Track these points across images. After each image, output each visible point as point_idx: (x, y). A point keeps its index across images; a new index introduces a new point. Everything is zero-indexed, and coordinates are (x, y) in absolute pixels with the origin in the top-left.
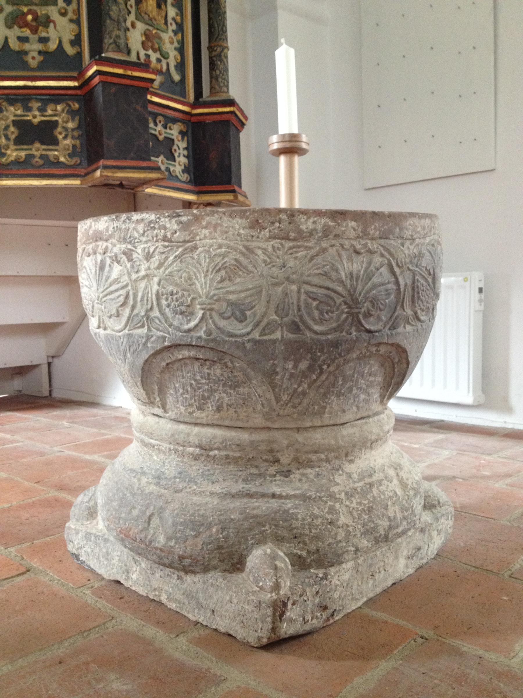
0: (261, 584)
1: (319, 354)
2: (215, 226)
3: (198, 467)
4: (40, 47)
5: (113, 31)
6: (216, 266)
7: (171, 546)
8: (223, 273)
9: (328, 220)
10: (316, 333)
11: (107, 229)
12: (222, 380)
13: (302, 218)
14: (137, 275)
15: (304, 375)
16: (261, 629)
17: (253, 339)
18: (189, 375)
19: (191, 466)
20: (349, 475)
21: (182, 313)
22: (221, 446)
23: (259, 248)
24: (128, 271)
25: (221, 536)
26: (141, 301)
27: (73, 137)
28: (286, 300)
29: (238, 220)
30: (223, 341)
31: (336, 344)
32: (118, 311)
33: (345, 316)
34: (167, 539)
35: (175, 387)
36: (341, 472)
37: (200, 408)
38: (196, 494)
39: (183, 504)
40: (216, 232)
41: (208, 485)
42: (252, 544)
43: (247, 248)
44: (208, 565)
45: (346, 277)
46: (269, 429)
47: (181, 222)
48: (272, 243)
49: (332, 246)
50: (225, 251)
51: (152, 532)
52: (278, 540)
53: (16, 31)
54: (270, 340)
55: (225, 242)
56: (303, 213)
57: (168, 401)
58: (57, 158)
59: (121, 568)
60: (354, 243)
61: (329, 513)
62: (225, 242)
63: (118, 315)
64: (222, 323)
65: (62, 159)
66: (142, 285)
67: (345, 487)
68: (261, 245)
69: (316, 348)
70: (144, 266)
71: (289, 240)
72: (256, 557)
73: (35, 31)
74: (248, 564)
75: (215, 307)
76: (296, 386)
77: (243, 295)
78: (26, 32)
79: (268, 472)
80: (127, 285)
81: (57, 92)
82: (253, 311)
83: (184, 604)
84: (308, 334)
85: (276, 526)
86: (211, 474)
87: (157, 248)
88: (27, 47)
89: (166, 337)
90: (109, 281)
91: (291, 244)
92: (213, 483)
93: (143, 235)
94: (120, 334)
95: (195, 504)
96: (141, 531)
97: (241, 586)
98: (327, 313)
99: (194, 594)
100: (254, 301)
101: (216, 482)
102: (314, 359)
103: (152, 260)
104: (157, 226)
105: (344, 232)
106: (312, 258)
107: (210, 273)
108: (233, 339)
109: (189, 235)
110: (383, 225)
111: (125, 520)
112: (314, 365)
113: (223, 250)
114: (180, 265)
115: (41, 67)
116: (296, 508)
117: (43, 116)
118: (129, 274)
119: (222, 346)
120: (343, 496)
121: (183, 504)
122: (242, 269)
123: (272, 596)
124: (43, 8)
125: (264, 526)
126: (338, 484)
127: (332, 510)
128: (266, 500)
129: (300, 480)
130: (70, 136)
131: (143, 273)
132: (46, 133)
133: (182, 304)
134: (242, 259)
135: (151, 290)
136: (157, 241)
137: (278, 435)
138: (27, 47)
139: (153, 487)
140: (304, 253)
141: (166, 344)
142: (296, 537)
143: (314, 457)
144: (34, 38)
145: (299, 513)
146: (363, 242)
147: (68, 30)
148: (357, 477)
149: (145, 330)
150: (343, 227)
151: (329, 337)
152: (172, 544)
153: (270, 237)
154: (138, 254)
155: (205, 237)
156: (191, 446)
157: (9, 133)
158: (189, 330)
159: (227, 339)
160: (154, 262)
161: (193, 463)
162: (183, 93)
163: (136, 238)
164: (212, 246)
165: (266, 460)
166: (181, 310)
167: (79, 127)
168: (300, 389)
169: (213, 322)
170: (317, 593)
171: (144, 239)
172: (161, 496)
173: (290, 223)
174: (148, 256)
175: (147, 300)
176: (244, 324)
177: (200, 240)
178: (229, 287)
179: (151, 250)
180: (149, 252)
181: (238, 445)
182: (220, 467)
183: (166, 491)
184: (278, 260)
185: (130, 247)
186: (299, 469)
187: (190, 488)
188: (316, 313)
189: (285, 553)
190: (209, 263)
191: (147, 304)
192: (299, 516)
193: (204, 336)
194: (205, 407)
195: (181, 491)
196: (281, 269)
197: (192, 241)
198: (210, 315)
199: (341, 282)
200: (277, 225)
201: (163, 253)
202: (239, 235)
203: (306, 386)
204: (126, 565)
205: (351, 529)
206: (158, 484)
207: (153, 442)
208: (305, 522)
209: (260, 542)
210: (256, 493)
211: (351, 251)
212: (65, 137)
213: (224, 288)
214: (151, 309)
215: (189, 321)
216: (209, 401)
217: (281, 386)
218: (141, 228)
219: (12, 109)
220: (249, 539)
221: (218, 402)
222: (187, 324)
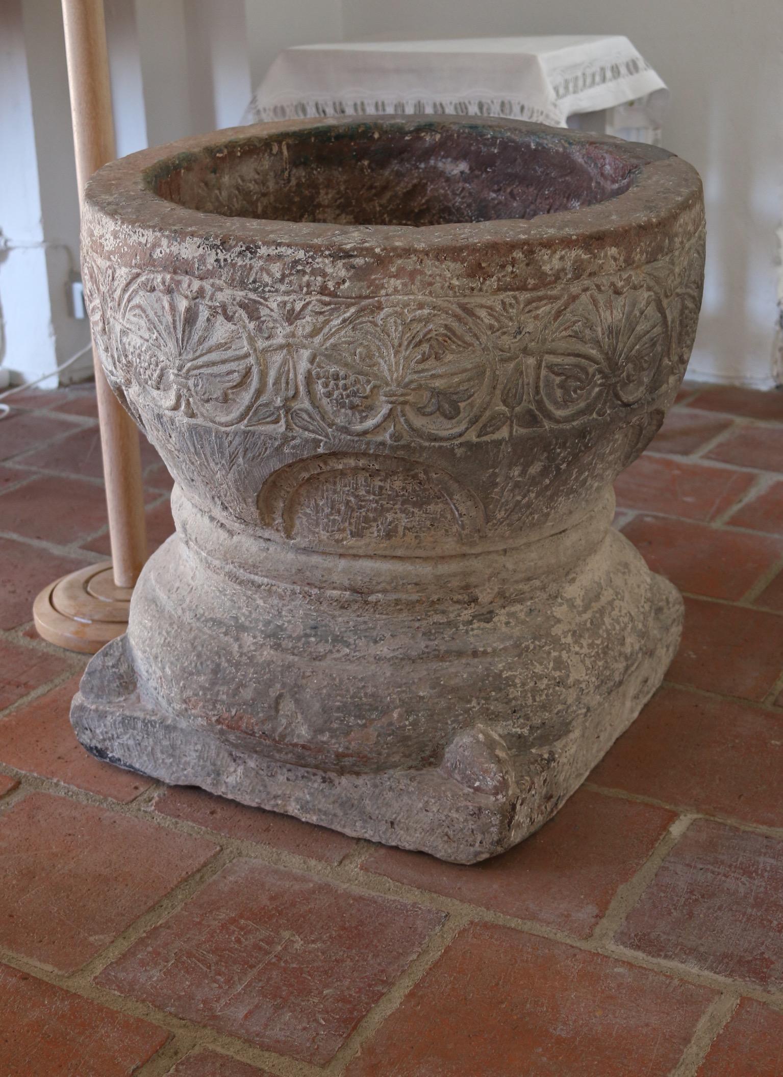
0: (477, 784)
1: (558, 450)
2: (412, 275)
3: (346, 619)
6: (413, 337)
7: (322, 742)
8: (425, 347)
9: (580, 252)
10: (558, 422)
11: (202, 259)
12: (403, 495)
13: (544, 254)
14: (267, 343)
15: (534, 481)
16: (481, 842)
17: (468, 442)
18: (347, 489)
19: (334, 617)
20: (571, 603)
21: (353, 407)
22: (388, 587)
23: (482, 306)
24: (249, 334)
25: (407, 723)
26: (274, 384)
28: (520, 381)
29: (450, 263)
30: (421, 447)
31: (582, 433)
32: (226, 394)
33: (597, 389)
34: (315, 731)
35: (317, 505)
36: (559, 600)
37: (357, 534)
38: (351, 662)
39: (334, 679)
40: (413, 283)
41: (367, 645)
42: (454, 728)
43: (463, 307)
44: (385, 763)
45: (603, 334)
46: (464, 555)
47: (353, 267)
48: (501, 297)
49: (585, 290)
50: (430, 314)
51: (284, 721)
52: (490, 719)
54: (492, 441)
55: (429, 299)
56: (545, 247)
57: (297, 522)
59: (203, 768)
60: (615, 279)
61: (554, 669)
62: (429, 299)
63: (226, 399)
64: (419, 422)
66: (278, 358)
67: (570, 623)
68: (483, 301)
69: (556, 444)
71: (526, 290)
72: (462, 745)
74: (447, 756)
75: (410, 398)
76: (519, 498)
77: (456, 379)
79: (461, 619)
80: (247, 356)
82: (469, 401)
83: (335, 815)
84: (547, 425)
85: (487, 699)
86: (369, 628)
87: (308, 304)
89: (321, 441)
90: (206, 345)
91: (528, 295)
92: (376, 642)
93: (281, 281)
94: (228, 429)
95: (354, 678)
96: (263, 722)
97: (443, 788)
98: (575, 392)
99: (356, 802)
100: (473, 386)
101: (381, 639)
102: (551, 459)
103: (299, 322)
104: (308, 271)
105: (601, 267)
106: (559, 313)
107: (403, 347)
108: (437, 444)
109: (368, 287)
110: (651, 242)
111: (229, 706)
112: (550, 466)
113: (426, 311)
114: (352, 334)
116: (510, 669)
118: (251, 340)
119: (418, 455)
120: (569, 639)
121: (334, 679)
122: (455, 339)
123: (497, 800)
125: (469, 702)
126: (559, 621)
127: (559, 664)
128: (464, 661)
129: (507, 623)
131: (279, 340)
133: (355, 394)
134: (455, 325)
135: (295, 368)
136: (309, 293)
137: (476, 564)
139: (267, 653)
140: (548, 308)
141: (320, 450)
142: (515, 712)
143: (525, 587)
145: (515, 676)
146: (625, 276)
148: (581, 604)
149: (281, 427)
150: (600, 259)
151: (575, 423)
152: (325, 739)
153: (499, 289)
154: (272, 310)
155: (396, 291)
156: (334, 588)
158: (365, 433)
159: (427, 444)
160: (304, 327)
161: (337, 613)
163: (267, 285)
164: (408, 305)
165: (458, 602)
166: (351, 402)
168: (524, 501)
169: (407, 421)
170: (545, 781)
171: (283, 288)
172: (289, 667)
173: (528, 265)
174: (292, 317)
175: (287, 383)
176: (454, 421)
177: (387, 295)
178: (435, 368)
179: (298, 306)
180: (293, 310)
181: (416, 584)
182: (384, 617)
183: (296, 659)
184: (511, 324)
185: (252, 296)
186: (504, 607)
187: (338, 651)
188: (559, 393)
189: (500, 736)
190: (403, 333)
191: (287, 389)
192: (517, 681)
193: (389, 442)
194: (366, 532)
195: (325, 656)
196: (515, 337)
197: (374, 297)
198: (402, 411)
199: (597, 343)
200: (509, 269)
201: (321, 313)
202: (451, 287)
203: (533, 495)
204: (214, 764)
205: (583, 686)
206: (277, 647)
207: (258, 579)
208: (526, 688)
209: (468, 724)
210: (449, 652)
211: (611, 292)
213: (427, 370)
214: (295, 396)
215: (363, 419)
216: (375, 524)
217: (498, 501)
218: (276, 269)
220: (449, 722)
221: (389, 525)
222: (361, 422)
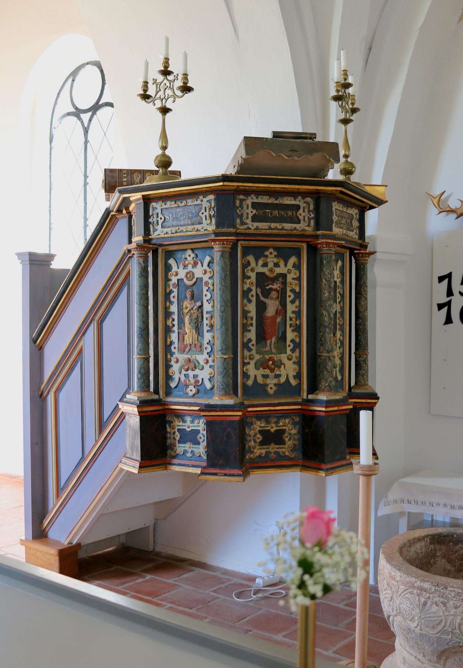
4: (275, 381)
5: (328, 378)
27: (294, 439)
53: (262, 371)
58: (284, 453)
65: (287, 454)
70: (453, 611)
73: (272, 370)
78: (267, 372)
81: (287, 412)
88: (268, 381)
115: (276, 393)
117: (277, 426)
124: (278, 356)
130: (292, 439)
132: (277, 438)
138: (268, 381)
144: (272, 375)
147: (292, 369)
149: (450, 637)
157: (256, 439)
162: (342, 387)
167: (298, 433)
171: (454, 599)
185: (446, 600)
212: (290, 439)
218: (453, 594)
219: (259, 423)
